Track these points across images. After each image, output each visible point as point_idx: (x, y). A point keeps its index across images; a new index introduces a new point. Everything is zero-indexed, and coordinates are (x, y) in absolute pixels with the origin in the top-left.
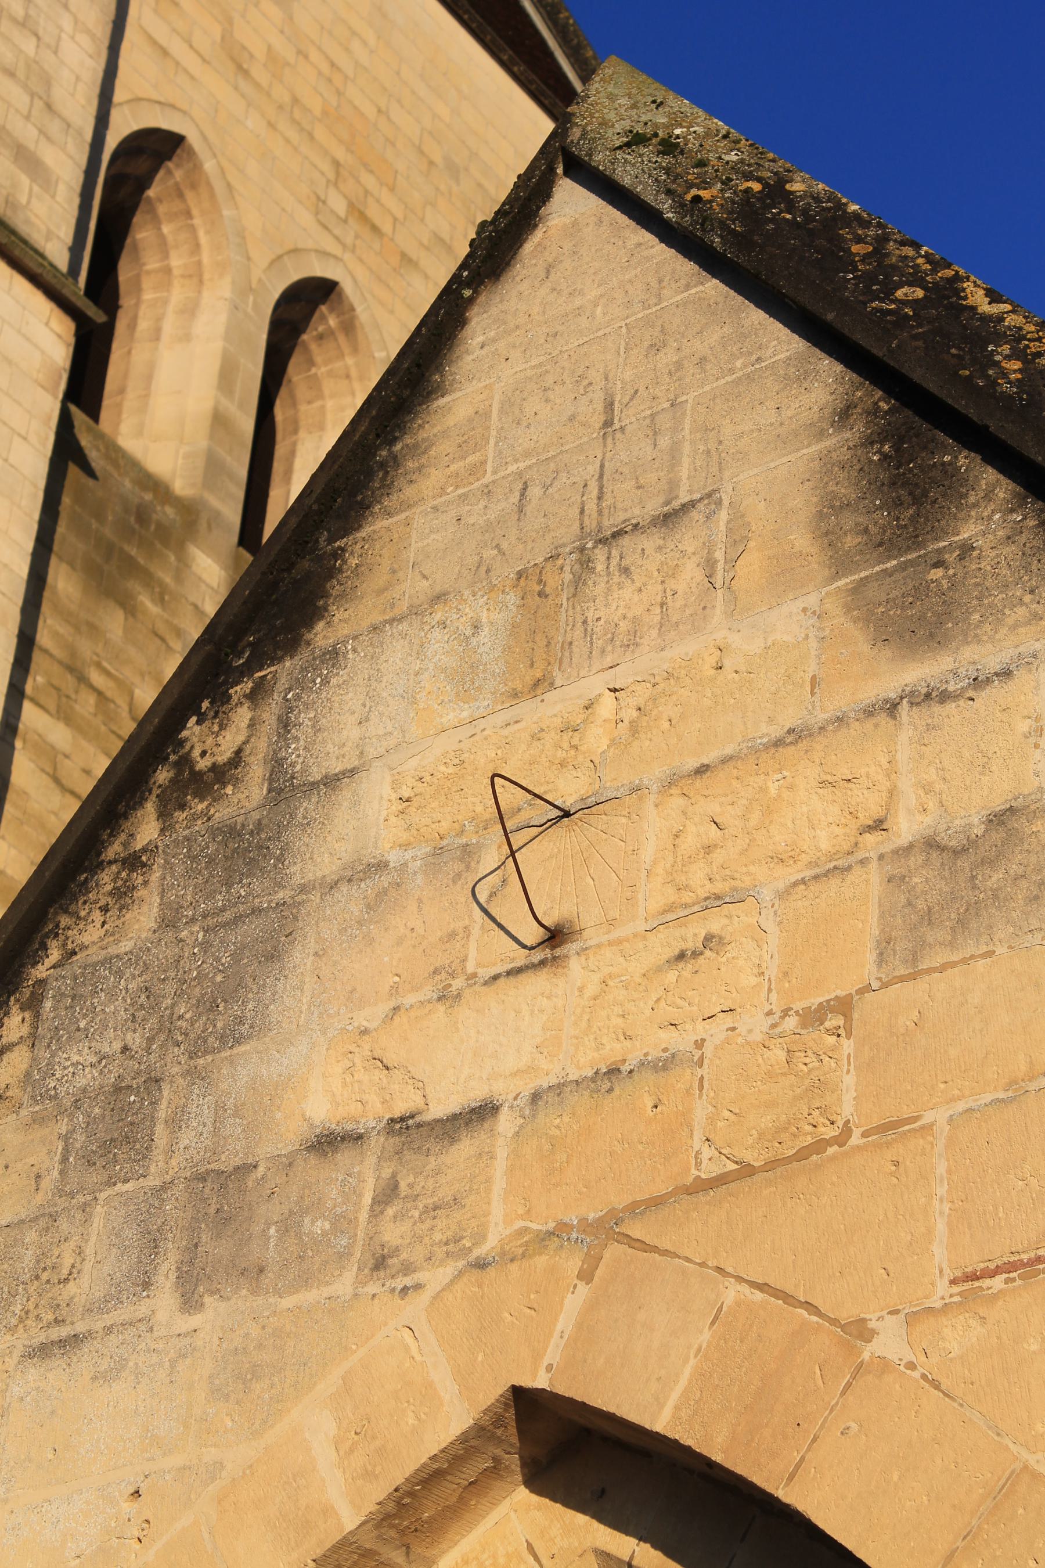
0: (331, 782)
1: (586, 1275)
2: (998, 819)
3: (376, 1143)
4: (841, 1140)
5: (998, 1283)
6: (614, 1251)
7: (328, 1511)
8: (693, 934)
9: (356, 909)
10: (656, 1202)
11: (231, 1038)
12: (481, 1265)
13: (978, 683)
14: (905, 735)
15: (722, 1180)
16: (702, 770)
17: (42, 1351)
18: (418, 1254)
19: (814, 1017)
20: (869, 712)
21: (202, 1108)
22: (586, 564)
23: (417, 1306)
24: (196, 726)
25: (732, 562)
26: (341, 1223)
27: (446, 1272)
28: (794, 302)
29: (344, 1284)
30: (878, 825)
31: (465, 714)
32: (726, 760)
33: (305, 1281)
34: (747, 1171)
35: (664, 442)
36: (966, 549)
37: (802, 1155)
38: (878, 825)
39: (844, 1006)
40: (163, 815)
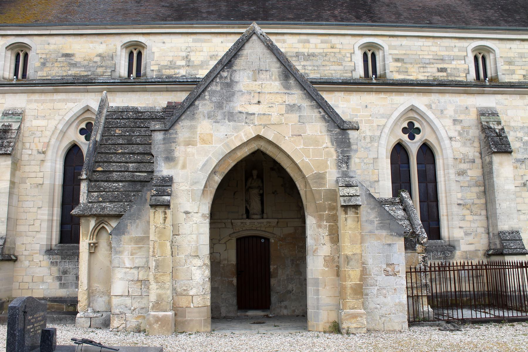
0: (237, 82)
1: (264, 128)
2: (294, 104)
3: (245, 113)
4: (283, 124)
5: (294, 136)
6: (266, 127)
7: (244, 140)
8: (271, 105)
9: (241, 94)
10: (269, 124)
11: (230, 101)
12: (255, 125)
13: (292, 94)
14: (287, 96)
15: (274, 124)
16: (270, 93)
17: (216, 122)
18: (249, 123)
19: (281, 114)
20: (284, 93)
21: (228, 106)
22: (259, 72)
23: (250, 127)
24: (311, 42)
25: (272, 77)
26: (242, 119)
27: (252, 125)
28: (69, 76)
29: (243, 124)
30: (285, 102)
31: (95, 315)
32: (273, 93)
33: (239, 123)
34: (276, 124)
35: (265, 63)
36: (291, 83)
37: (280, 124)
38: (285, 102)
39: (283, 114)
40: (219, 79)
